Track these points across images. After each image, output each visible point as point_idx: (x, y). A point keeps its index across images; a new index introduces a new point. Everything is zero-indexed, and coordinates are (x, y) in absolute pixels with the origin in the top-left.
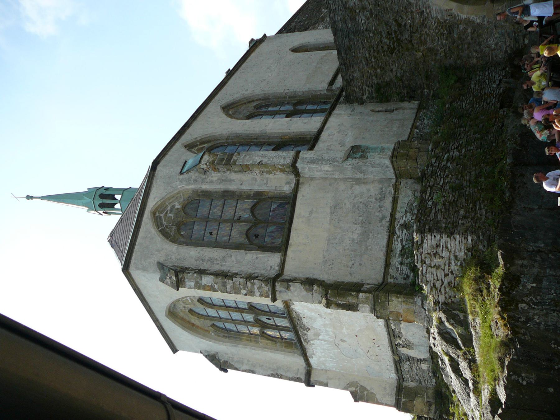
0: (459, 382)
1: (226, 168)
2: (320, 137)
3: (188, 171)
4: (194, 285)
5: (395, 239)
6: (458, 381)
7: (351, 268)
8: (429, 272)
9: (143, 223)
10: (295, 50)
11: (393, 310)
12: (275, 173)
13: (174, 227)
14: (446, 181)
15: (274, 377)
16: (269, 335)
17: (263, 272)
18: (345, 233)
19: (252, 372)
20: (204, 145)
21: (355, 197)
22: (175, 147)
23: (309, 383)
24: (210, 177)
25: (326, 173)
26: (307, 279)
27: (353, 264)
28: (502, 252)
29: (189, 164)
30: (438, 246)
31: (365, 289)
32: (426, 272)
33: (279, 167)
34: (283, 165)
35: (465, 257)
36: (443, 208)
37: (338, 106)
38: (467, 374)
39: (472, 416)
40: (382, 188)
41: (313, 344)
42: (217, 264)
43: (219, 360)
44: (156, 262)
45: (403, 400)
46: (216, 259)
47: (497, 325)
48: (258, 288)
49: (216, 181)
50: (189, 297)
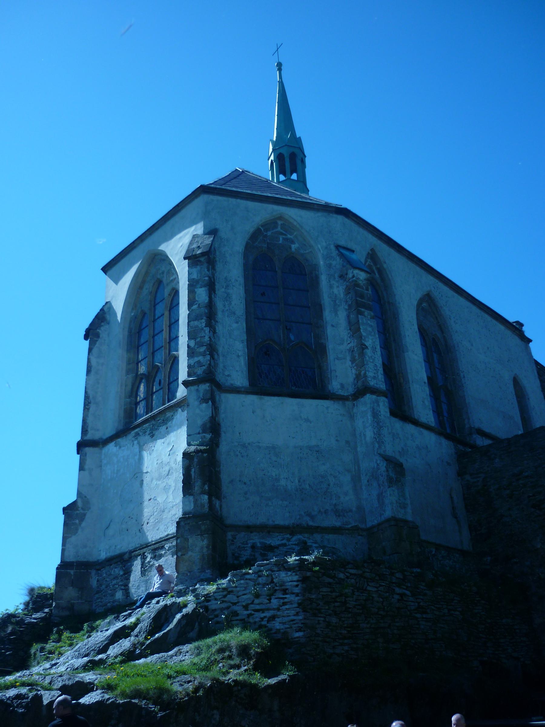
0: (102, 641)
1: (352, 303)
2: (408, 424)
3: (342, 255)
4: (194, 279)
5: (286, 536)
6: (104, 639)
7: (240, 481)
8: (247, 583)
9: (267, 205)
10: (516, 382)
11: (190, 541)
12: (353, 367)
13: (266, 246)
14: (374, 595)
15: (85, 400)
16: (138, 387)
17: (221, 366)
18: (285, 468)
19: (89, 371)
20: (377, 274)
21: (335, 477)
22: (370, 236)
23: (81, 446)
24: (337, 285)
25: (362, 434)
26: (219, 425)
27: (245, 483)
28: (287, 681)
29: (351, 255)
30: (285, 592)
31: (214, 503)
32: (246, 579)
33: (363, 372)
34: (365, 376)
35: (273, 631)
36: (337, 594)
37: (452, 443)
38: (113, 651)
39: (58, 663)
40: (351, 511)
41: (133, 444)
42: (224, 306)
43: (99, 326)
44: (217, 227)
45: (72, 572)
46: (230, 304)
47: (185, 682)
48: (199, 362)
49: (333, 292)
50: (176, 276)
